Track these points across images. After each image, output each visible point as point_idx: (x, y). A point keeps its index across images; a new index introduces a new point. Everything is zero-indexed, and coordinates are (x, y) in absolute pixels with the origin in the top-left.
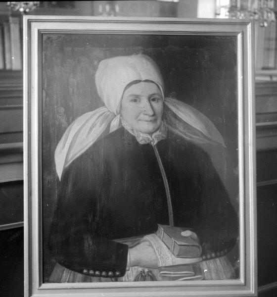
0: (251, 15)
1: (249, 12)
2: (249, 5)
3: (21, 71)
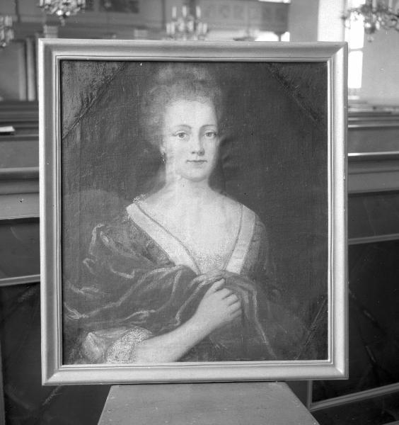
0: (393, 20)
1: (390, 14)
2: (390, 5)
3: (36, 102)
